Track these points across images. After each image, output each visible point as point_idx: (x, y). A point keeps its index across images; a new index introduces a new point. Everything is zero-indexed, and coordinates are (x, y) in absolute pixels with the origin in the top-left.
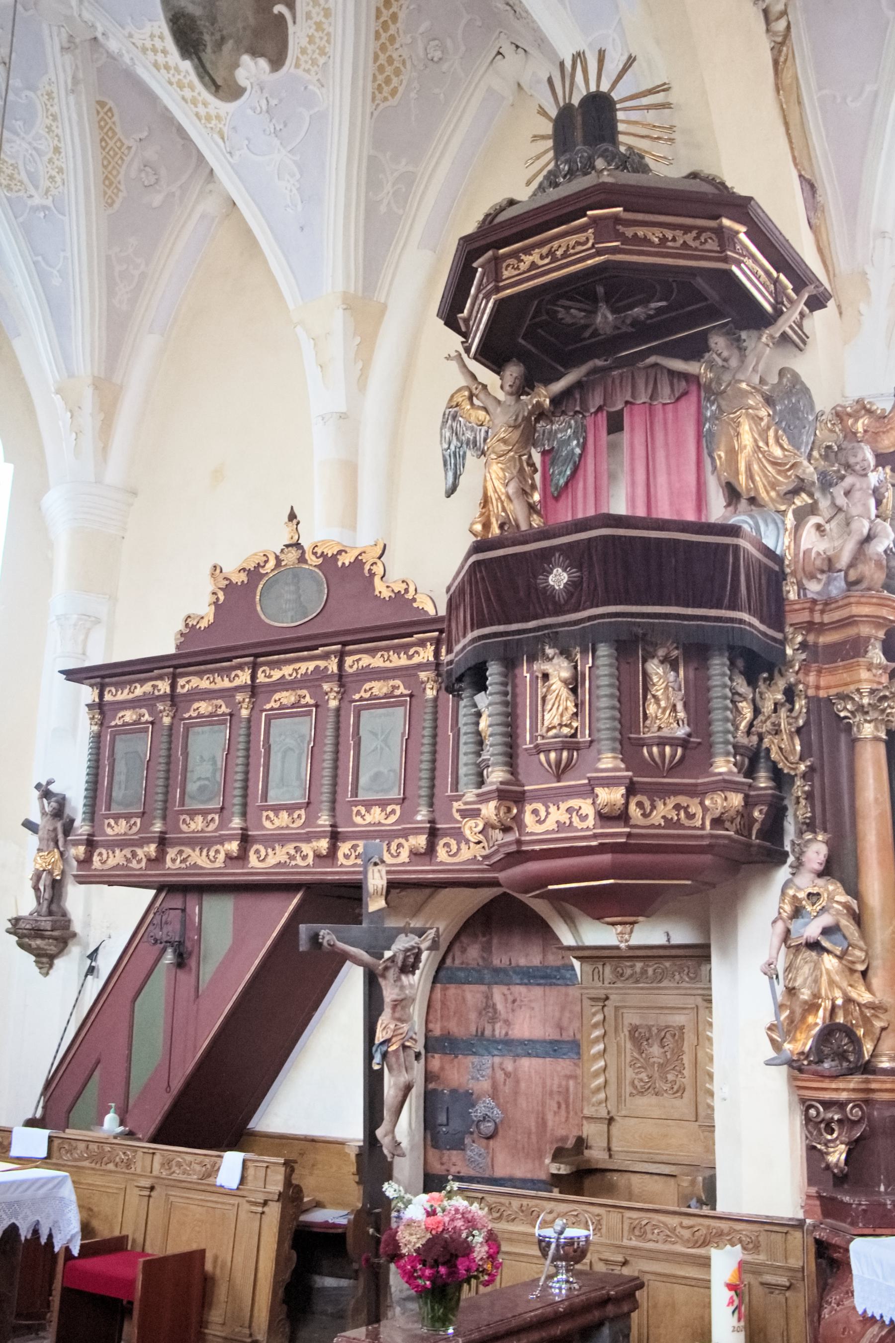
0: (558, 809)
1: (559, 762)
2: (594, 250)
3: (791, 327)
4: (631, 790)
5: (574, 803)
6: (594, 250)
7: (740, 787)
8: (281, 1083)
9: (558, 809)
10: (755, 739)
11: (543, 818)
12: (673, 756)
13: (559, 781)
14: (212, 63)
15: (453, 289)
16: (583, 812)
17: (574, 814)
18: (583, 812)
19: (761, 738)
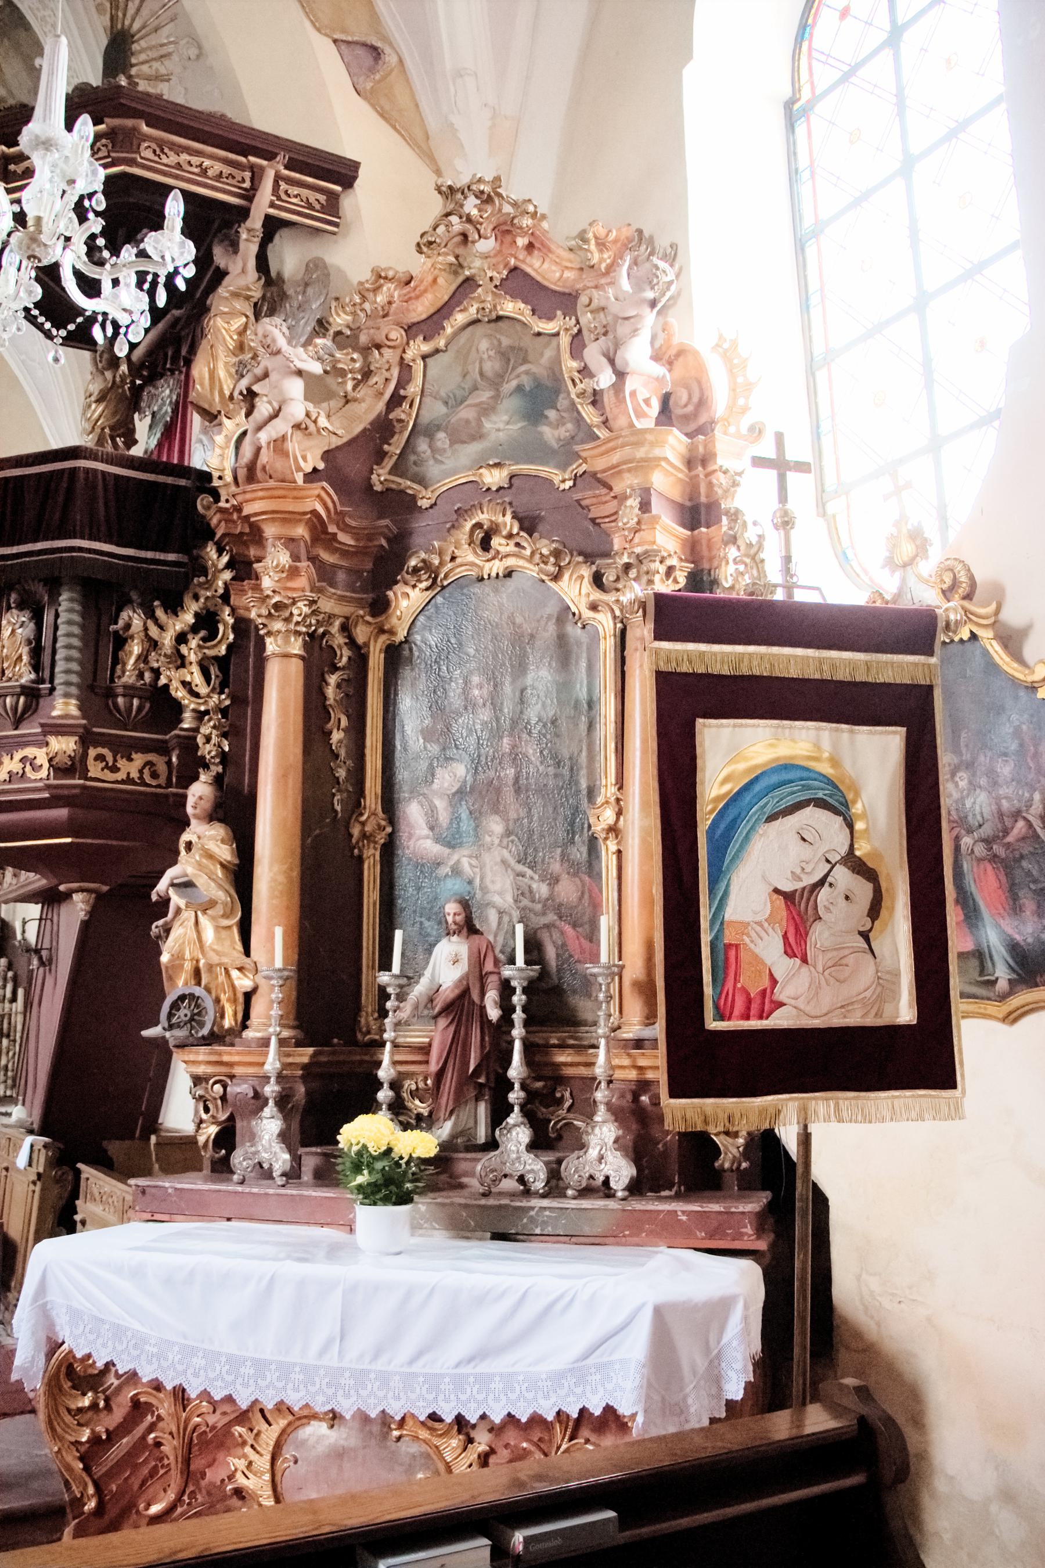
0: (12, 758)
1: (15, 708)
2: (109, 160)
3: (272, 205)
4: (87, 739)
5: (30, 751)
6: (109, 160)
7: (74, 730)
8: (296, 808)
9: (12, 758)
10: (148, 676)
11: (147, 768)
12: (140, 709)
13: (16, 729)
14: (11, 251)
15: (707, 1193)
16: (38, 762)
17: (110, 764)
18: (38, 762)
19: (157, 673)
